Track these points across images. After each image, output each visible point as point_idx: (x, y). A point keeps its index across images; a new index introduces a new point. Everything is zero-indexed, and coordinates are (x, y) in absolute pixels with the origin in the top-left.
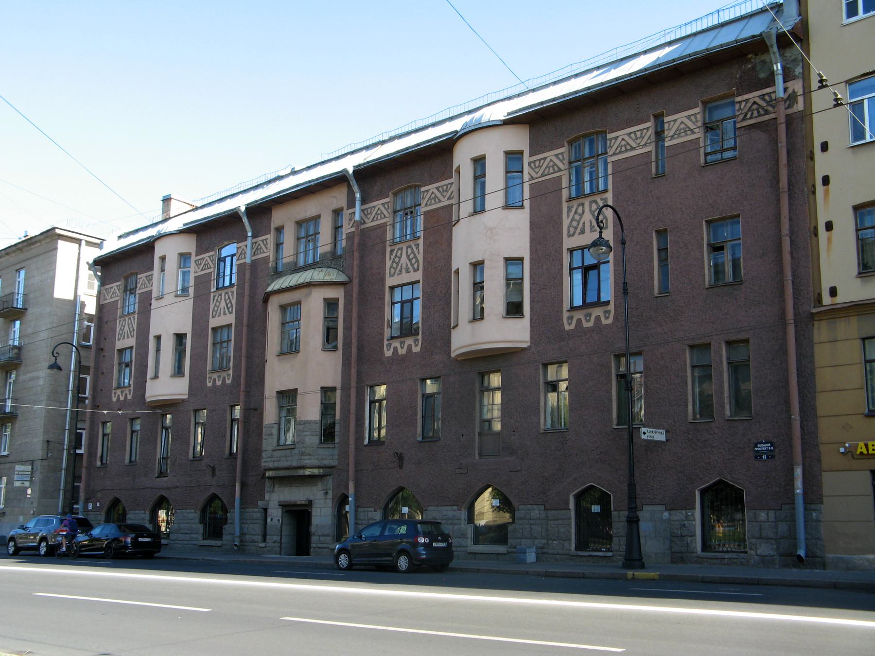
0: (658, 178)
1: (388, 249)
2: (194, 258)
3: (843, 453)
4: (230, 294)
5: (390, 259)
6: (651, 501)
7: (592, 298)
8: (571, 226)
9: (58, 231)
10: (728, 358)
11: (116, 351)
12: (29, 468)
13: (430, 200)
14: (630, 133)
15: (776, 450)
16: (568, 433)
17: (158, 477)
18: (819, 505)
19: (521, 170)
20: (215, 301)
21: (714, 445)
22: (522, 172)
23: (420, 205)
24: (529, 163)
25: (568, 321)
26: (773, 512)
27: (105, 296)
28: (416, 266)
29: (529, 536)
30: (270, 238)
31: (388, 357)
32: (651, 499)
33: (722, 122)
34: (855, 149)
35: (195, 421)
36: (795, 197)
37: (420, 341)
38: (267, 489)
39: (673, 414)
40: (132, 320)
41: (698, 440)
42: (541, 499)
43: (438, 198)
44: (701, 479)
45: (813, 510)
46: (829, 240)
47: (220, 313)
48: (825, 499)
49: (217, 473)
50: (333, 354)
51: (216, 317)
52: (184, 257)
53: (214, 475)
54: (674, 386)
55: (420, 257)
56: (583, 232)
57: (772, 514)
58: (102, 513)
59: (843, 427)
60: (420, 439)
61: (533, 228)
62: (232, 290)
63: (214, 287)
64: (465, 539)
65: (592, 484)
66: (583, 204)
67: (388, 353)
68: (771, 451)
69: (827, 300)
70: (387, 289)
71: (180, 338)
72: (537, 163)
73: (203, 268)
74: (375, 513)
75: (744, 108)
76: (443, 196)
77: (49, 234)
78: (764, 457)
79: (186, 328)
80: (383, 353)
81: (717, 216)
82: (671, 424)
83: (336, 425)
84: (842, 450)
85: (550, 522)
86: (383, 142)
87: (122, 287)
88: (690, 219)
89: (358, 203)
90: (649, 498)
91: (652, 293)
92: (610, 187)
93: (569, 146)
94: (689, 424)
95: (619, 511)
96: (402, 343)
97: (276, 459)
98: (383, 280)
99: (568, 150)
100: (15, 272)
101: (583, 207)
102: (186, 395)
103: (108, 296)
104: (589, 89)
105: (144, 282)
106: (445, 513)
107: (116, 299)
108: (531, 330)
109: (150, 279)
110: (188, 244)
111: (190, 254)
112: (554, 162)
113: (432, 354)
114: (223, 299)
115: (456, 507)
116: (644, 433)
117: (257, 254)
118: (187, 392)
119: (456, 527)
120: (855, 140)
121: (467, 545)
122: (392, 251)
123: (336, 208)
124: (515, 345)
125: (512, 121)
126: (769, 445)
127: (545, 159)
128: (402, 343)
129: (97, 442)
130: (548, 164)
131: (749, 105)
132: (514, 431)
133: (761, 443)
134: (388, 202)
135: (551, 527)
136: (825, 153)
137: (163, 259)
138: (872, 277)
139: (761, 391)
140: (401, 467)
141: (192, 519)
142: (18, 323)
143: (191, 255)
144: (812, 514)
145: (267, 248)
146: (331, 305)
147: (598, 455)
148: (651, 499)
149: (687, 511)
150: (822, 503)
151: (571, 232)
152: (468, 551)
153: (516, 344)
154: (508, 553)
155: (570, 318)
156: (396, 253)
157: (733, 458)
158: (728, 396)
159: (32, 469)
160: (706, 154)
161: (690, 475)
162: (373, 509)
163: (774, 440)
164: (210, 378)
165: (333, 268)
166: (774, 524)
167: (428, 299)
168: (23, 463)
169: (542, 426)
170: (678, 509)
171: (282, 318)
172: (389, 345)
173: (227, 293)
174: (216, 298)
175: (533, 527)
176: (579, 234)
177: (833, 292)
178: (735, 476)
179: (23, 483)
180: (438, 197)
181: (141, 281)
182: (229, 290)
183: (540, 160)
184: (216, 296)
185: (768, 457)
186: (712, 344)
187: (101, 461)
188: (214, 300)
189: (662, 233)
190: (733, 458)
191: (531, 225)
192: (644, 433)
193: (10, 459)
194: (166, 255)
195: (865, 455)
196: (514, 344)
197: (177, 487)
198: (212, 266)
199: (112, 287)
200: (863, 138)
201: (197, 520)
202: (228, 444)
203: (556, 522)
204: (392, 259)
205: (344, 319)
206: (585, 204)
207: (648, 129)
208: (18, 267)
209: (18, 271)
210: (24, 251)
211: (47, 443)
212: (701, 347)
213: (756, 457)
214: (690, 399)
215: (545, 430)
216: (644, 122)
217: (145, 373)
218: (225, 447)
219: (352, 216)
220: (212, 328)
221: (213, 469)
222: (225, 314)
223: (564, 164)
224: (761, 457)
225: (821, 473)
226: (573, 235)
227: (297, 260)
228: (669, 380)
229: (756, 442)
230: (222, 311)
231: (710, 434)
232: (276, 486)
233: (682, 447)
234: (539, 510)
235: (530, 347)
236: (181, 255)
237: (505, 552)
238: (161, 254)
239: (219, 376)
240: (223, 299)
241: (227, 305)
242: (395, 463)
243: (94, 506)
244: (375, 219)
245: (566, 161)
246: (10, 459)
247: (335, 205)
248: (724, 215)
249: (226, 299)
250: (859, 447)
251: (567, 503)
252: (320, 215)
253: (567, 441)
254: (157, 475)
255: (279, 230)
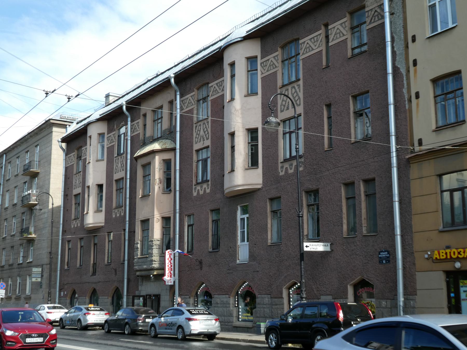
0: (354, 58)
1: (194, 126)
2: (106, 136)
3: (427, 258)
4: (297, 87)
5: (195, 132)
6: (324, 292)
7: (205, 179)
8: (282, 105)
9: (52, 121)
10: (365, 192)
11: (73, 196)
12: (40, 269)
13: (306, 49)
14: (342, 24)
15: (391, 256)
16: (281, 246)
17: (92, 275)
18: (414, 296)
19: (256, 69)
20: (116, 163)
21: (357, 253)
22: (257, 70)
23: (299, 54)
24: (261, 63)
25: (281, 169)
26: (390, 301)
27: (68, 162)
28: (207, 136)
29: (263, 316)
30: (140, 121)
31: (208, 193)
32: (324, 291)
33: (361, 25)
34: (431, 39)
35: (109, 240)
36: (398, 76)
37: (210, 186)
38: (140, 283)
39: (335, 232)
40: (207, 125)
41: (349, 250)
42: (269, 290)
43: (217, 91)
44: (351, 277)
45: (412, 300)
46: (418, 104)
47: (118, 170)
48: (418, 292)
49: (118, 273)
50: (168, 195)
51: (117, 173)
52: (251, 60)
53: (116, 274)
54: (335, 212)
55: (209, 130)
56: (288, 109)
57: (389, 302)
58: (67, 299)
59: (427, 240)
60: (211, 250)
61: (263, 108)
62: (298, 84)
63: (116, 154)
64: (232, 318)
65: (294, 280)
66: (288, 90)
67: (195, 194)
68: (388, 257)
69: (417, 148)
70: (194, 152)
71: (100, 187)
72: (315, 38)
73: (269, 69)
74: (189, 299)
75: (370, 15)
76: (219, 89)
77: (48, 123)
78: (384, 262)
79: (103, 181)
80: (192, 195)
81: (357, 92)
82: (334, 239)
83: (171, 241)
84: (426, 256)
85: (274, 307)
86: (149, 81)
87: (76, 156)
88: (343, 95)
89: (129, 123)
90: (323, 291)
91: (324, 148)
92: (301, 76)
93: (282, 50)
94: (343, 238)
95: (309, 299)
96: (201, 187)
97: (141, 264)
98: (192, 146)
99: (281, 53)
100: (35, 147)
101: (288, 91)
102: (103, 223)
103: (185, 106)
104: (286, 12)
105: (190, 101)
106: (222, 300)
107: (73, 163)
108: (263, 176)
109: (221, 86)
110: (102, 128)
111: (256, 57)
112: (340, 30)
113: (215, 193)
114: (120, 161)
115: (227, 296)
116: (307, 246)
117: (135, 132)
118: (104, 221)
119: (228, 309)
120: (433, 32)
121: (233, 321)
122: (196, 127)
123: (170, 100)
124: (252, 187)
125: (249, 37)
126: (387, 253)
127: (268, 60)
128: (201, 187)
129: (65, 254)
130: (270, 63)
131: (373, 13)
132: (255, 244)
133: (382, 252)
134: (194, 95)
135: (274, 310)
136: (414, 43)
137: (232, 65)
138: (441, 131)
139: (382, 214)
140: (201, 268)
141: (106, 303)
142: (36, 178)
143: (104, 134)
144: (410, 303)
145: (139, 128)
146: (167, 164)
147: (297, 260)
148: (324, 291)
149: (344, 299)
150: (416, 295)
151: (282, 109)
152: (233, 326)
153: (254, 186)
154: (253, 327)
155: (282, 167)
156: (198, 128)
157: (368, 263)
158: (366, 218)
159: (42, 270)
160: (353, 49)
161: (345, 274)
162: (188, 296)
163: (390, 250)
164: (114, 212)
165: (169, 139)
166: (390, 309)
167: (213, 158)
168: (37, 266)
169: (269, 241)
170: (338, 298)
171: (143, 172)
172: (282, 167)
173: (204, 124)
174: (117, 161)
175: (265, 309)
176: (286, 110)
177: (420, 142)
178: (369, 275)
179: (37, 279)
180: (312, 43)
181: (84, 151)
182: (295, 85)
183: (266, 61)
184: (197, 126)
185: (386, 262)
186: (355, 182)
187: (68, 266)
188: (115, 162)
189: (329, 106)
190: (368, 263)
191: (262, 106)
192: (307, 246)
193: (33, 264)
194: (234, 61)
195: (439, 259)
196: (252, 186)
197: (99, 282)
198: (114, 141)
199: (71, 156)
200: (437, 30)
201: (109, 304)
202: (122, 254)
203: (276, 307)
204: (196, 132)
205: (106, 194)
206: (289, 89)
207: (320, 34)
208: (26, 150)
209: (36, 146)
210: (38, 134)
211: (50, 254)
212: (349, 185)
213: (380, 262)
214: (107, 253)
215: (272, 244)
216: (318, 30)
217: (223, 169)
218: (121, 256)
219: (267, 63)
220: (115, 180)
221: (116, 271)
222: (120, 171)
223: (278, 63)
224: (383, 262)
225: (415, 273)
226: (283, 111)
227: (153, 135)
228: (333, 208)
229: (380, 251)
230: (77, 186)
231: (355, 246)
232: (144, 281)
233: (340, 254)
234: (268, 298)
235: (262, 187)
236: (100, 134)
237: (251, 327)
238: (230, 61)
239: (118, 211)
240: (120, 161)
241: (121, 165)
242: (199, 266)
243: (64, 293)
244: (188, 106)
245: (280, 61)
246: (33, 264)
247: (169, 99)
248: (361, 91)
249: (293, 92)
250: (435, 255)
251: (281, 293)
252: (162, 105)
253: (281, 251)
254: (91, 274)
255: (145, 115)
